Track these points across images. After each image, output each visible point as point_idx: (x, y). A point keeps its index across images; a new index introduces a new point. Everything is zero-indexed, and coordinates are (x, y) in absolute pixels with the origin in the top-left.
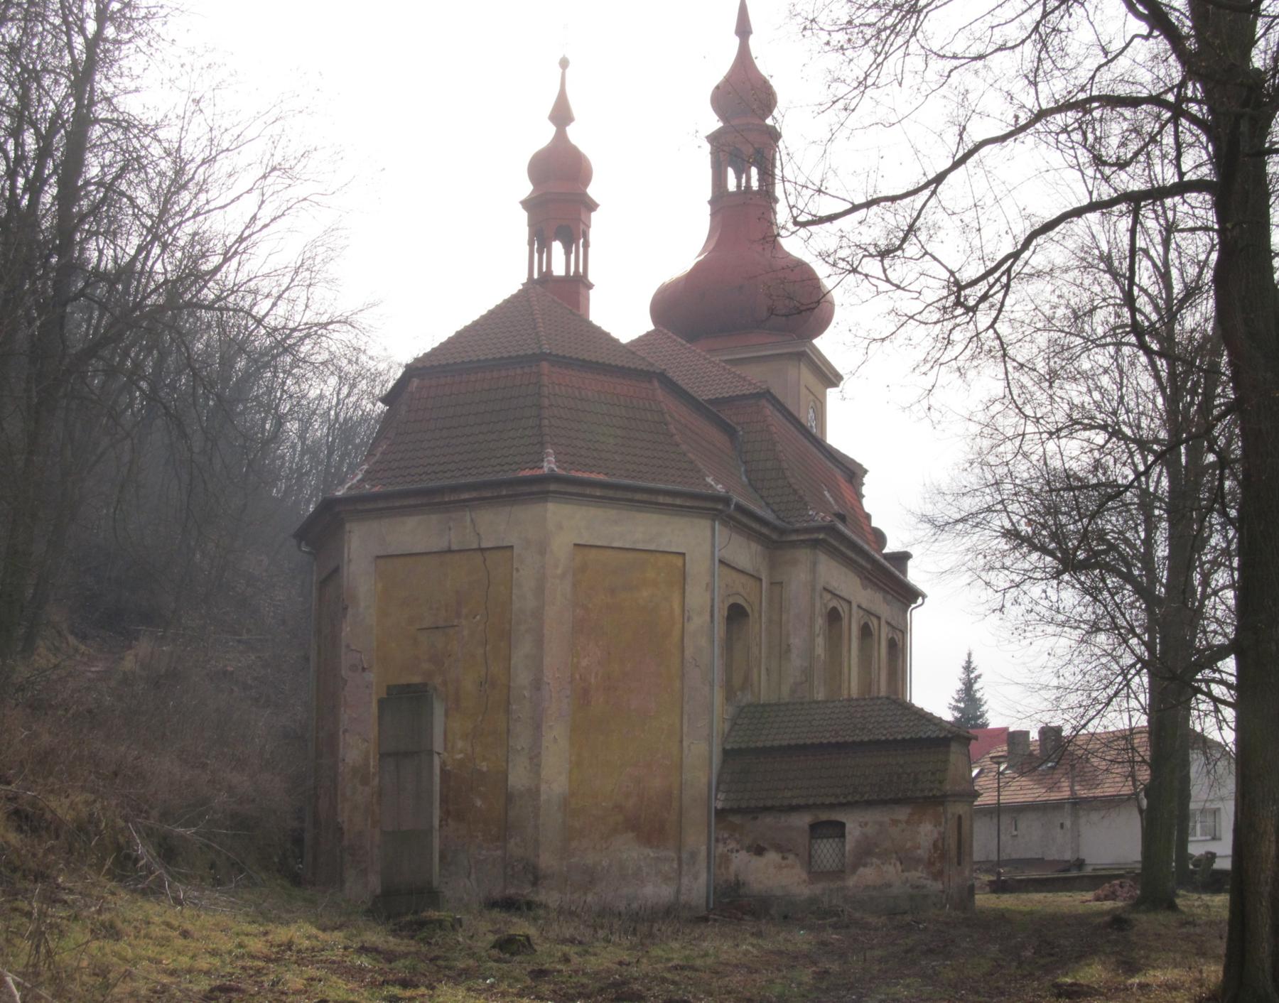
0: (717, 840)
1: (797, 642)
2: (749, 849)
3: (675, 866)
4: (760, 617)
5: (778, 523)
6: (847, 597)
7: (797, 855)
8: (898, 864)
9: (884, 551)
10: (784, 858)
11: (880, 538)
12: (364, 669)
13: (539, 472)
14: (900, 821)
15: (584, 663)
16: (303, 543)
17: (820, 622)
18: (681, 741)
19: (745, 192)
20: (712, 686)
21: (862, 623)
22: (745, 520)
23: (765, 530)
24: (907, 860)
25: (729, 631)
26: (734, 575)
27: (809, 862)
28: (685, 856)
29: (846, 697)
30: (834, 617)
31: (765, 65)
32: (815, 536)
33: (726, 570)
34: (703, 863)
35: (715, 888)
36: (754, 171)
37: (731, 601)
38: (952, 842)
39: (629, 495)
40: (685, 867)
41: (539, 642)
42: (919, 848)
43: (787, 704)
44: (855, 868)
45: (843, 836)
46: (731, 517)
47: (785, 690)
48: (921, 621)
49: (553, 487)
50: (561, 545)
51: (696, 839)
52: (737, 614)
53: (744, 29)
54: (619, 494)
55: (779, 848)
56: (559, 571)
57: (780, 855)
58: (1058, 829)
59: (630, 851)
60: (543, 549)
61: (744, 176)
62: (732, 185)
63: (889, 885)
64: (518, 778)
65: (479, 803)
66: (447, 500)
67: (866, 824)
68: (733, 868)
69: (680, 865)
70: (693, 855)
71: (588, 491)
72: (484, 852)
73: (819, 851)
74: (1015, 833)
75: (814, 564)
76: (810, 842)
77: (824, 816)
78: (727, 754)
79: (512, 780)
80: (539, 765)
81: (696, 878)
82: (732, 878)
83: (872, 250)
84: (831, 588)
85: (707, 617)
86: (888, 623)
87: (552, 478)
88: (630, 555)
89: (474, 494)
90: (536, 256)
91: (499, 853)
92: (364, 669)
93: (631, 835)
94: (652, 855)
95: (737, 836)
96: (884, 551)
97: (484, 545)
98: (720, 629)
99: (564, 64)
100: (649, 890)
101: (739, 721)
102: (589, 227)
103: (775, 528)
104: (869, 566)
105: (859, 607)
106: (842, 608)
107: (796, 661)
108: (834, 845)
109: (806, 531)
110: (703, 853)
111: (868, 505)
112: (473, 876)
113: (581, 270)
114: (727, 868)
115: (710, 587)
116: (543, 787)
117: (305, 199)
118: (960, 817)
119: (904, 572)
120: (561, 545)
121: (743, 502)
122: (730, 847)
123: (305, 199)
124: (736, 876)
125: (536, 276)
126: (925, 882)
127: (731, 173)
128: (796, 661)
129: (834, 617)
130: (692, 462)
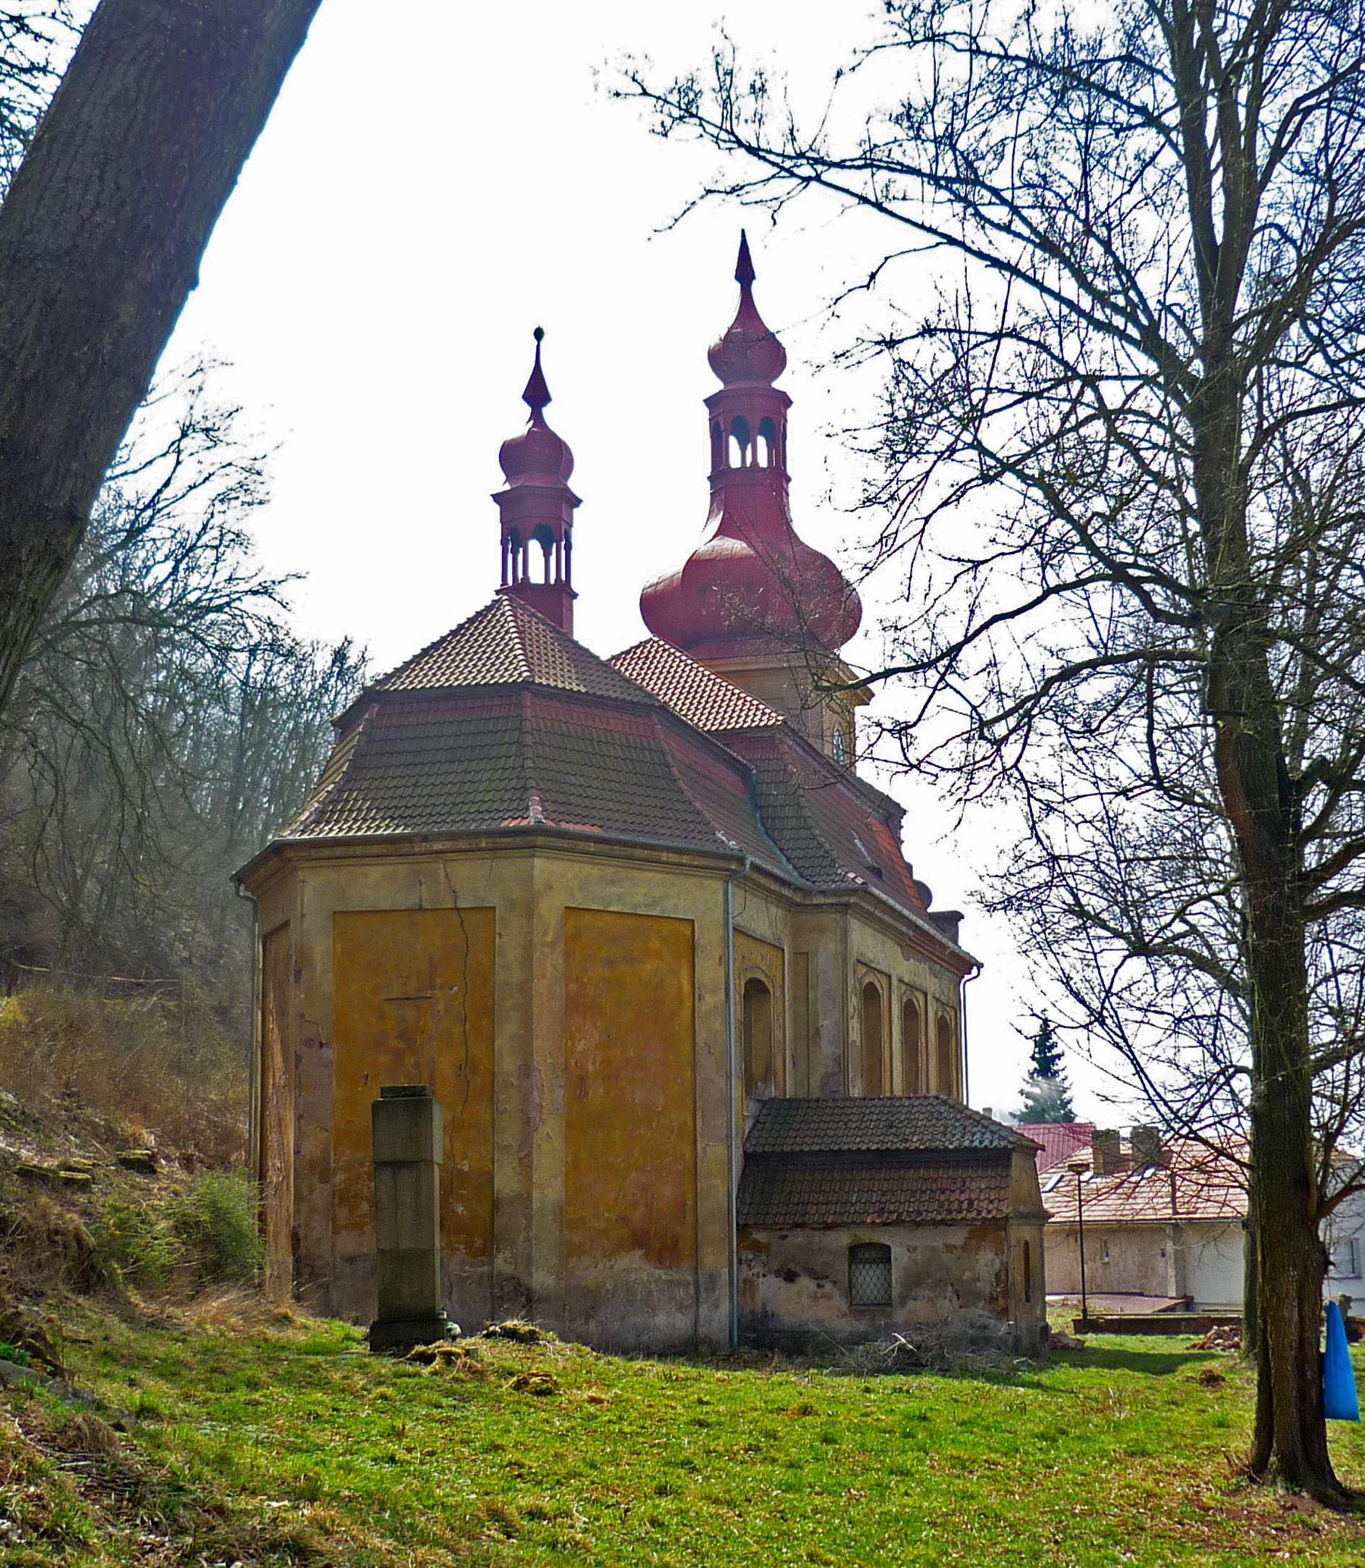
0: (740, 1262)
1: (826, 1024)
2: (778, 1273)
3: (692, 1292)
4: (783, 994)
5: (800, 882)
6: (885, 969)
7: (835, 1283)
8: (955, 1298)
9: (929, 910)
10: (819, 1286)
11: (924, 894)
12: (321, 1045)
13: (524, 823)
14: (955, 1247)
15: (580, 1046)
16: (242, 887)
17: (854, 1001)
18: (695, 1143)
19: (751, 471)
20: (729, 1077)
21: (905, 999)
22: (763, 880)
23: (785, 892)
24: (966, 1295)
25: (747, 1012)
26: (752, 945)
27: (850, 1291)
28: (701, 1281)
29: (888, 1094)
30: (870, 994)
31: (771, 314)
32: (844, 899)
33: (741, 940)
34: (723, 1291)
35: (739, 1320)
36: (761, 441)
37: (749, 975)
38: (1017, 1276)
39: (628, 851)
40: (703, 1295)
41: (527, 1021)
42: (978, 1280)
43: (817, 1101)
44: (904, 1300)
45: (887, 1260)
46: (745, 877)
47: (815, 1082)
48: (975, 992)
49: (540, 840)
50: (550, 909)
51: (715, 1259)
52: (755, 990)
53: (745, 272)
54: (617, 850)
55: (812, 1273)
56: (549, 939)
57: (815, 1283)
58: (1159, 1257)
59: (633, 1265)
60: (529, 912)
61: (749, 447)
62: (735, 461)
63: (945, 1322)
64: (506, 1182)
65: (460, 1209)
66: (417, 849)
67: (915, 1249)
68: (759, 1297)
69: (697, 1291)
70: (713, 1280)
71: (581, 845)
72: (467, 1268)
73: (861, 1280)
74: (1106, 1259)
75: (845, 933)
76: (850, 1266)
77: (866, 1236)
78: (750, 1158)
79: (498, 1183)
80: (530, 1166)
81: (717, 1307)
82: (759, 1309)
83: (888, 725)
84: (866, 961)
85: (722, 996)
86: (937, 1000)
87: (537, 830)
88: (632, 922)
89: (448, 845)
90: (510, 556)
91: (484, 1269)
92: (321, 1045)
93: (639, 1253)
94: (664, 1277)
95: (764, 1257)
96: (929, 910)
97: (461, 904)
98: (736, 1011)
99: (539, 334)
100: (661, 1320)
101: (761, 1120)
102: (571, 526)
103: (797, 889)
104: (911, 933)
105: (901, 981)
106: (881, 984)
107: (827, 1049)
108: (878, 1272)
109: (836, 893)
110: (725, 1277)
111: (909, 852)
112: (454, 1297)
113: (563, 577)
114: (753, 1298)
115: (724, 960)
116: (535, 1194)
117: (230, 464)
118: (1027, 1244)
119: (955, 939)
120: (550, 909)
121: (758, 862)
122: (755, 1271)
123: (230, 464)
124: (764, 1306)
125: (510, 582)
126: (988, 1321)
127: (733, 442)
128: (827, 1049)
129: (870, 994)
130: (699, 813)
